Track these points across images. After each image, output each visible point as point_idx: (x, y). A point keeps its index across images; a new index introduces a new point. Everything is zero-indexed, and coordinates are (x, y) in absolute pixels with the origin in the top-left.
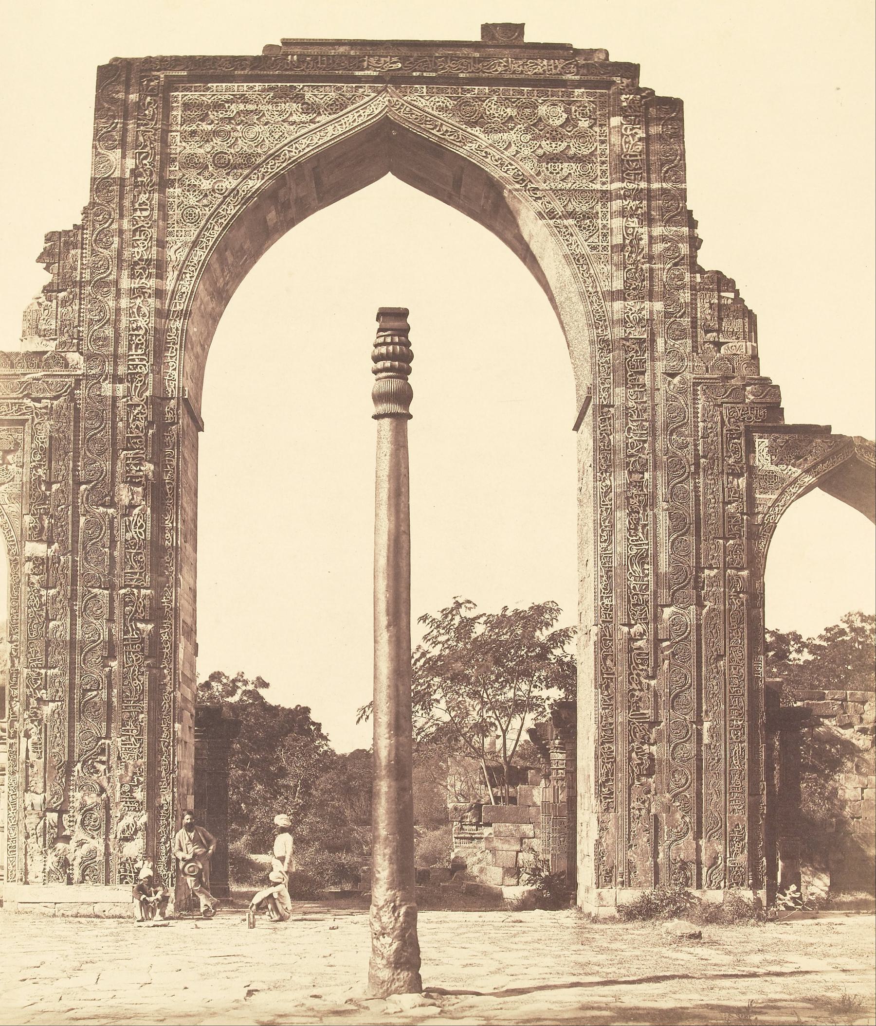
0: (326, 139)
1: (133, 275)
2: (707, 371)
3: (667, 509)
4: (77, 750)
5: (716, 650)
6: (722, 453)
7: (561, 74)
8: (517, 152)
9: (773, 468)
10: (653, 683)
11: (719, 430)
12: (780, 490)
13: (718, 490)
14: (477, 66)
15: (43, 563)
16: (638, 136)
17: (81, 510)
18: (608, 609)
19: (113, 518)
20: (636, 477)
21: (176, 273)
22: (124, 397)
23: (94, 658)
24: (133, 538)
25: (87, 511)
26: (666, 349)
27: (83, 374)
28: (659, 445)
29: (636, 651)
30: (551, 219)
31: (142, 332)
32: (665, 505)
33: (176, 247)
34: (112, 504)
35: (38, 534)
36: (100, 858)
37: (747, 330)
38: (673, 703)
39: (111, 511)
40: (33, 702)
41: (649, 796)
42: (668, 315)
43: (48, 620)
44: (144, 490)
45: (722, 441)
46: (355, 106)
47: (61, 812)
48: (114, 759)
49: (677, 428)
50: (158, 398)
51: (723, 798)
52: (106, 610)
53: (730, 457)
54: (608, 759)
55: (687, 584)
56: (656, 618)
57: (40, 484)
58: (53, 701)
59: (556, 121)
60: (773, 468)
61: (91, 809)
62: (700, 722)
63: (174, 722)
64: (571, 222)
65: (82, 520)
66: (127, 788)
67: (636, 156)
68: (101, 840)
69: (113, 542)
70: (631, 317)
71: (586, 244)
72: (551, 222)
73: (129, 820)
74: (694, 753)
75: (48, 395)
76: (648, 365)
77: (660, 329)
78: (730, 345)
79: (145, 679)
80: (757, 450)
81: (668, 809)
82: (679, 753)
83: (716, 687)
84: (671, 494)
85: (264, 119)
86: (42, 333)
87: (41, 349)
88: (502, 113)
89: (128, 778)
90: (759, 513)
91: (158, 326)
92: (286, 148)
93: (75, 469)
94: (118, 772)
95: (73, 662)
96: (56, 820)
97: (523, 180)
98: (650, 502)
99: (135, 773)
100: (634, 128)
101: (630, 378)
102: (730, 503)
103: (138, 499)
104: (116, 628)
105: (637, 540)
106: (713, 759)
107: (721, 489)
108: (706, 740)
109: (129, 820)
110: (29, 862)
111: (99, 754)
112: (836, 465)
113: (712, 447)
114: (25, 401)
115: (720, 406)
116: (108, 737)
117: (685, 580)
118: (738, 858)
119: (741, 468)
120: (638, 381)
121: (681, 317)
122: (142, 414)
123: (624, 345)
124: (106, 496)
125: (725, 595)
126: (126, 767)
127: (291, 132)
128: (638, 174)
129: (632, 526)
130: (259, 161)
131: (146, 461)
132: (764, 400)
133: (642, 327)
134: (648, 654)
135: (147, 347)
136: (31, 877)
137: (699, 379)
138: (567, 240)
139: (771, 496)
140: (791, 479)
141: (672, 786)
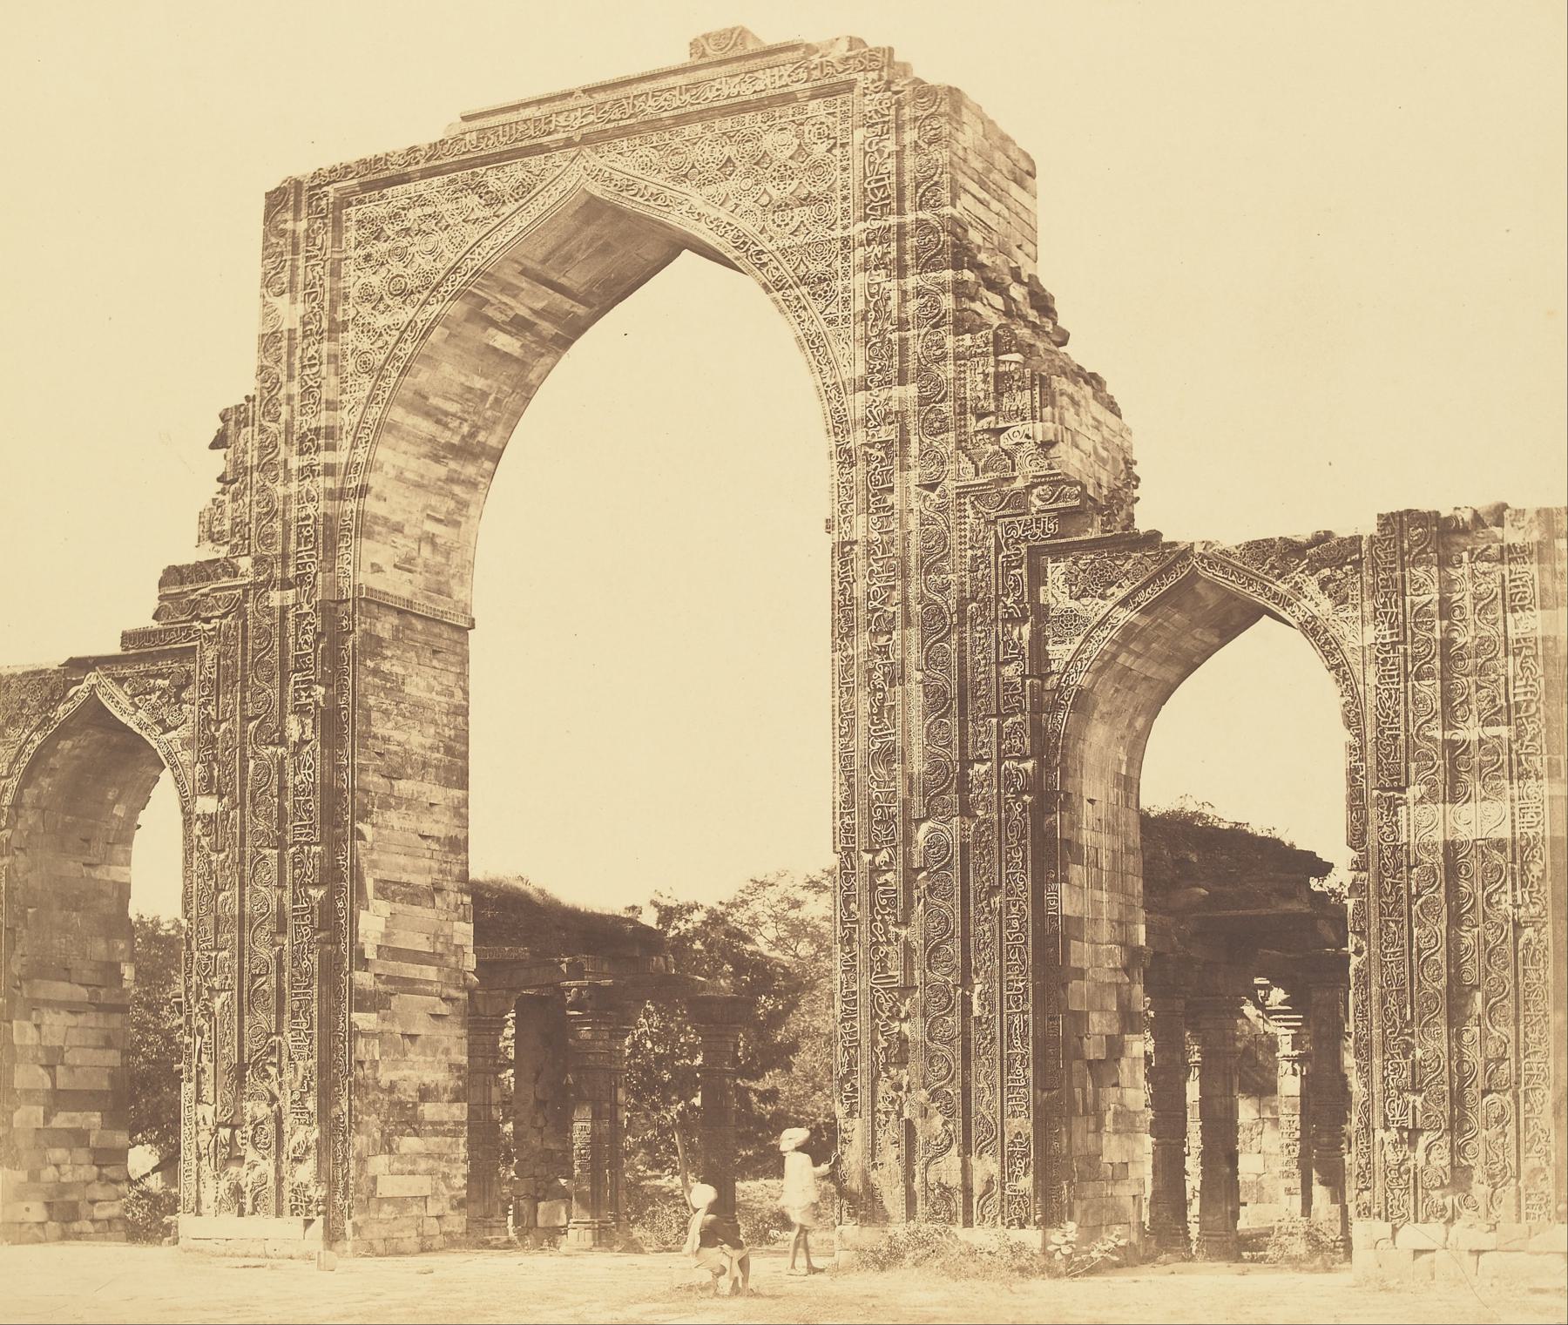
0: (512, 235)
1: (301, 449)
2: (977, 475)
3: (922, 682)
4: (246, 1050)
5: (988, 879)
6: (997, 590)
7: (787, 85)
8: (737, 206)
9: (1073, 604)
10: (903, 932)
11: (992, 558)
12: (1082, 637)
13: (989, 646)
14: (683, 98)
15: (211, 820)
16: (887, 151)
17: (249, 753)
18: (849, 829)
19: (283, 758)
20: (882, 640)
21: (350, 439)
22: (294, 605)
23: (262, 935)
24: (302, 782)
25: (256, 753)
26: (921, 450)
27: (250, 583)
28: (913, 590)
29: (880, 888)
30: (778, 290)
31: (311, 522)
32: (919, 676)
33: (349, 407)
34: (283, 742)
35: (210, 786)
36: (271, 1183)
37: (1037, 404)
38: (929, 960)
39: (280, 751)
40: (206, 995)
41: (900, 1093)
42: (923, 401)
43: (219, 890)
44: (314, 720)
45: (997, 574)
46: (544, 183)
47: (234, 1127)
48: (285, 1060)
49: (935, 562)
50: (333, 601)
51: (999, 1096)
52: (275, 875)
53: (1007, 596)
54: (850, 1042)
55: (948, 787)
56: (908, 839)
57: (209, 723)
58: (225, 990)
59: (785, 152)
60: (1073, 604)
61: (262, 1123)
62: (966, 982)
63: (350, 1011)
64: (805, 289)
65: (252, 764)
66: (296, 1096)
67: (883, 179)
68: (272, 1162)
69: (282, 788)
70: (875, 413)
71: (821, 317)
72: (778, 295)
73: (299, 1136)
74: (958, 1029)
75: (217, 613)
76: (896, 479)
77: (912, 423)
78: (1010, 431)
79: (314, 958)
80: (1049, 580)
81: (925, 1113)
82: (939, 1031)
83: (988, 934)
84: (926, 659)
85: (443, 223)
86: (216, 536)
87: (213, 556)
88: (718, 155)
89: (298, 1083)
90: (1052, 673)
91: (329, 512)
92: (468, 256)
93: (243, 702)
94: (287, 1076)
95: (241, 942)
96: (228, 1137)
97: (744, 243)
98: (896, 676)
99: (305, 1078)
100: (881, 141)
101: (872, 500)
102: (1007, 663)
103: (308, 734)
104: (288, 895)
105: (881, 730)
106: (985, 1038)
107: (993, 645)
108: (977, 1011)
109: (299, 1136)
110: (202, 1189)
111: (268, 1054)
112: (1164, 588)
113: (984, 584)
114: (195, 623)
115: (994, 522)
116: (279, 1032)
117: (945, 781)
118: (1020, 1182)
119: (1023, 610)
120: (885, 502)
121: (941, 401)
122: (311, 624)
123: (866, 453)
124: (275, 732)
125: (999, 799)
126: (296, 1070)
127: (473, 233)
128: (887, 205)
129: (875, 710)
130: (438, 278)
131: (315, 683)
132: (1054, 506)
133: (890, 424)
134: (895, 891)
135: (316, 540)
136: (203, 1209)
137: (963, 487)
138: (799, 317)
139: (1069, 646)
140: (1099, 618)
141: (930, 1079)
